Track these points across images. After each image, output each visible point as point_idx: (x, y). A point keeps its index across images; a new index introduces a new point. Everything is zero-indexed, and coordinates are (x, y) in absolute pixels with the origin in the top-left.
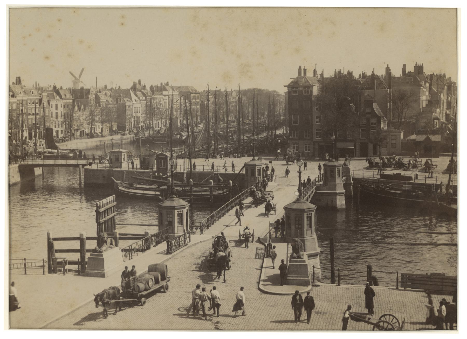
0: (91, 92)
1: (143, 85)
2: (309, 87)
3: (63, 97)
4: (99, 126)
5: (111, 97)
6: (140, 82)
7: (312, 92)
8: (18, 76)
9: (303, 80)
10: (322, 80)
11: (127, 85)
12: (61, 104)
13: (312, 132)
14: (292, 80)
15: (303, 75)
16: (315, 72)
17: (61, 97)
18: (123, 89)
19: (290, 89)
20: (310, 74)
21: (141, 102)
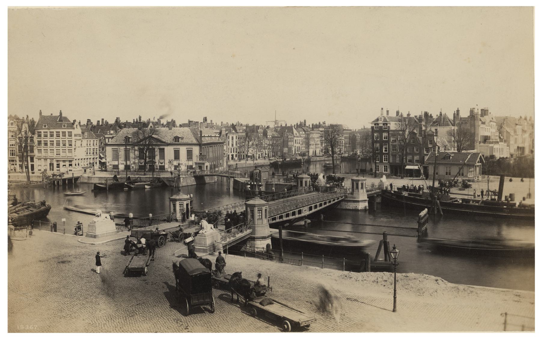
3: (238, 131)
6: (205, 119)
12: (236, 136)
17: (236, 131)
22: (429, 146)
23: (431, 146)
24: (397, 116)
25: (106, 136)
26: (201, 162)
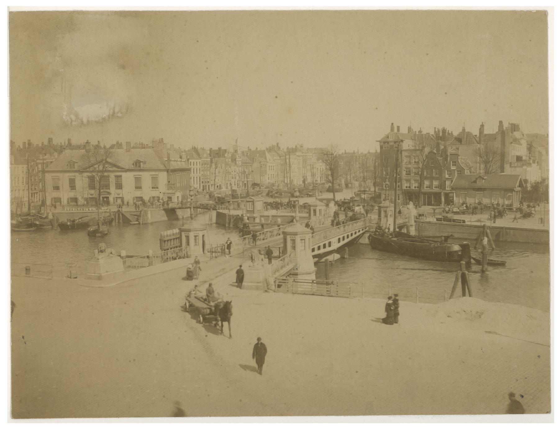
22: (452, 168)
23: (455, 168)
24: (409, 133)
25: (38, 161)
26: (170, 191)
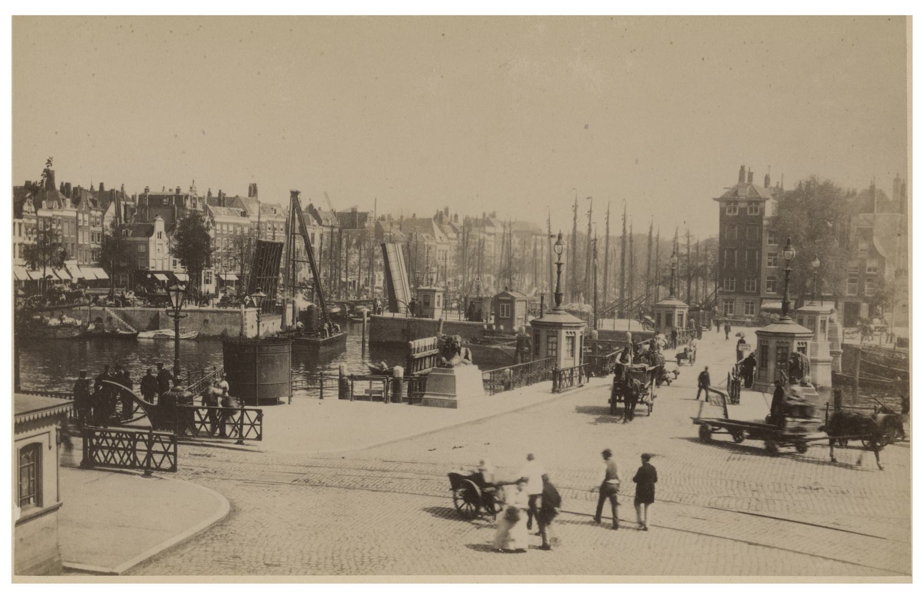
0: (368, 219)
1: (453, 215)
2: (756, 202)
4: (379, 276)
5: (401, 230)
7: (762, 212)
8: (253, 182)
9: (748, 189)
10: (778, 192)
11: (427, 212)
13: (759, 282)
14: (727, 190)
15: (746, 181)
16: (767, 179)
17: (320, 222)
18: (420, 219)
19: (724, 204)
20: (758, 182)
21: (450, 241)
